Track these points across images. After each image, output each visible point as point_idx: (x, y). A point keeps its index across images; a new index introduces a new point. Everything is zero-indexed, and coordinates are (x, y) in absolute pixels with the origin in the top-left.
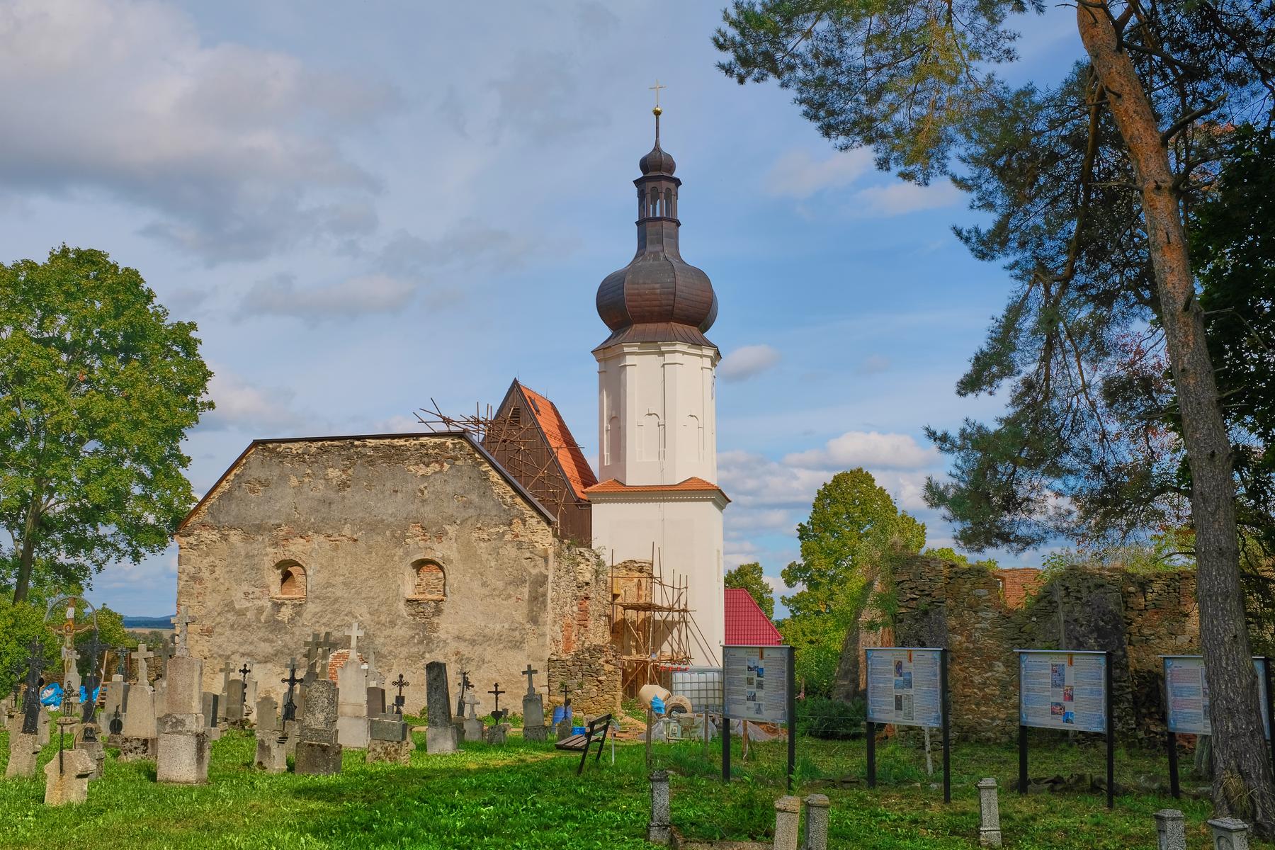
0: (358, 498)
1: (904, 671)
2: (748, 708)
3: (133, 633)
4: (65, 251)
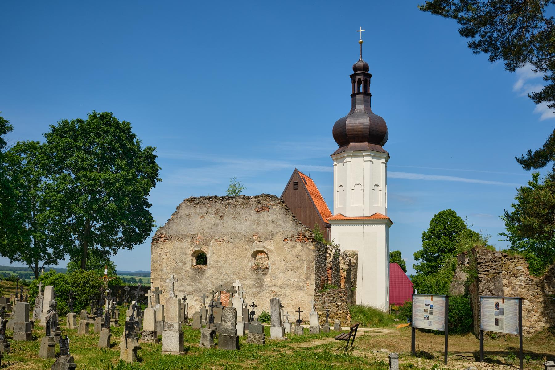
2: (425, 323)
4: (95, 116)
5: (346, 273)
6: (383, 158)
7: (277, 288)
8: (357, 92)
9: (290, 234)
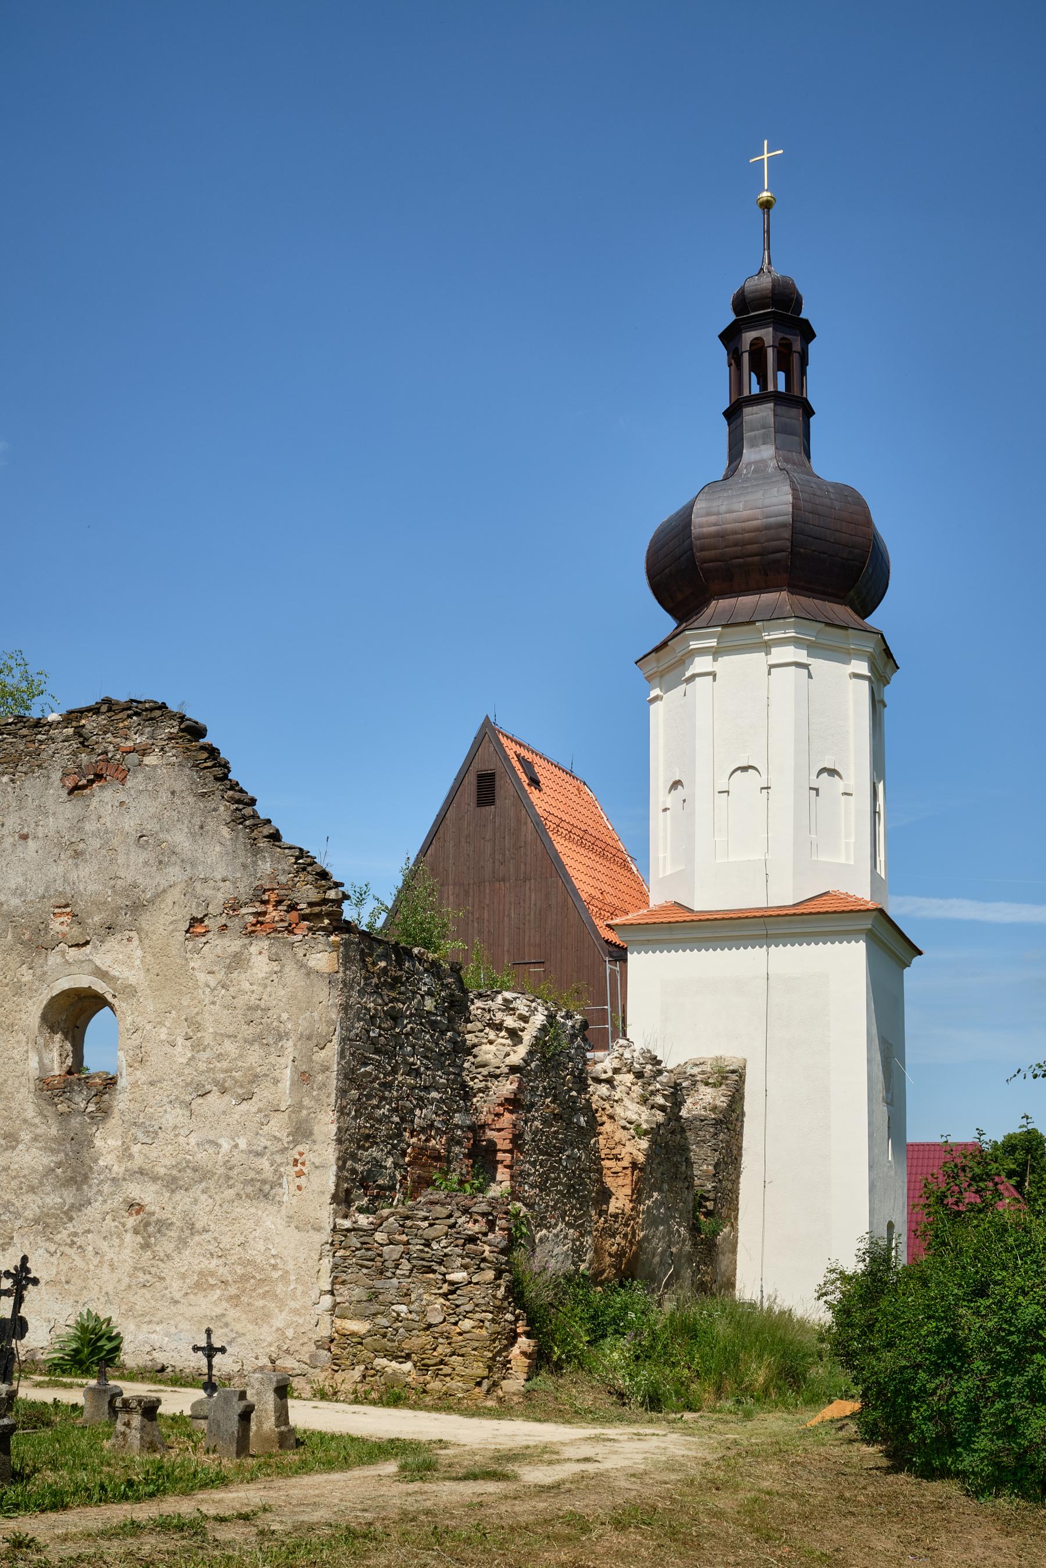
5: (644, 1144)
6: (859, 655)
7: (153, 1187)
8: (746, 393)
9: (220, 897)
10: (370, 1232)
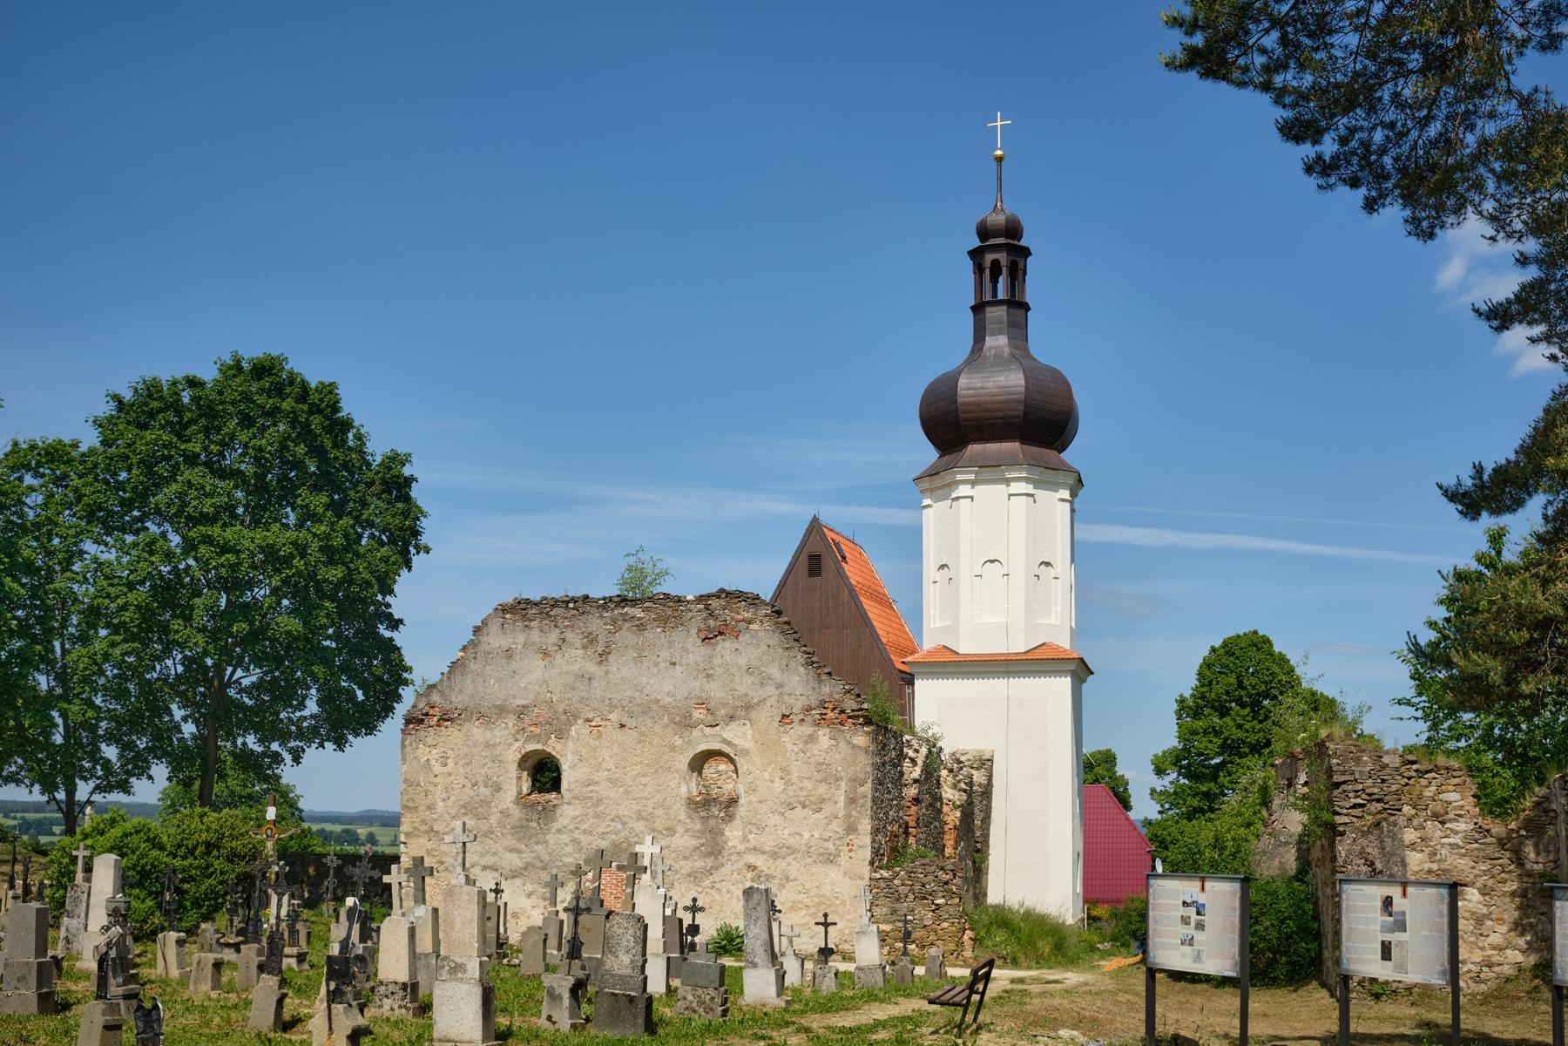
0: (625, 672)
1: (1395, 908)
2: (1183, 955)
3: (323, 830)
6: (1064, 486)
8: (988, 297)
9: (799, 704)
10: (891, 880)
